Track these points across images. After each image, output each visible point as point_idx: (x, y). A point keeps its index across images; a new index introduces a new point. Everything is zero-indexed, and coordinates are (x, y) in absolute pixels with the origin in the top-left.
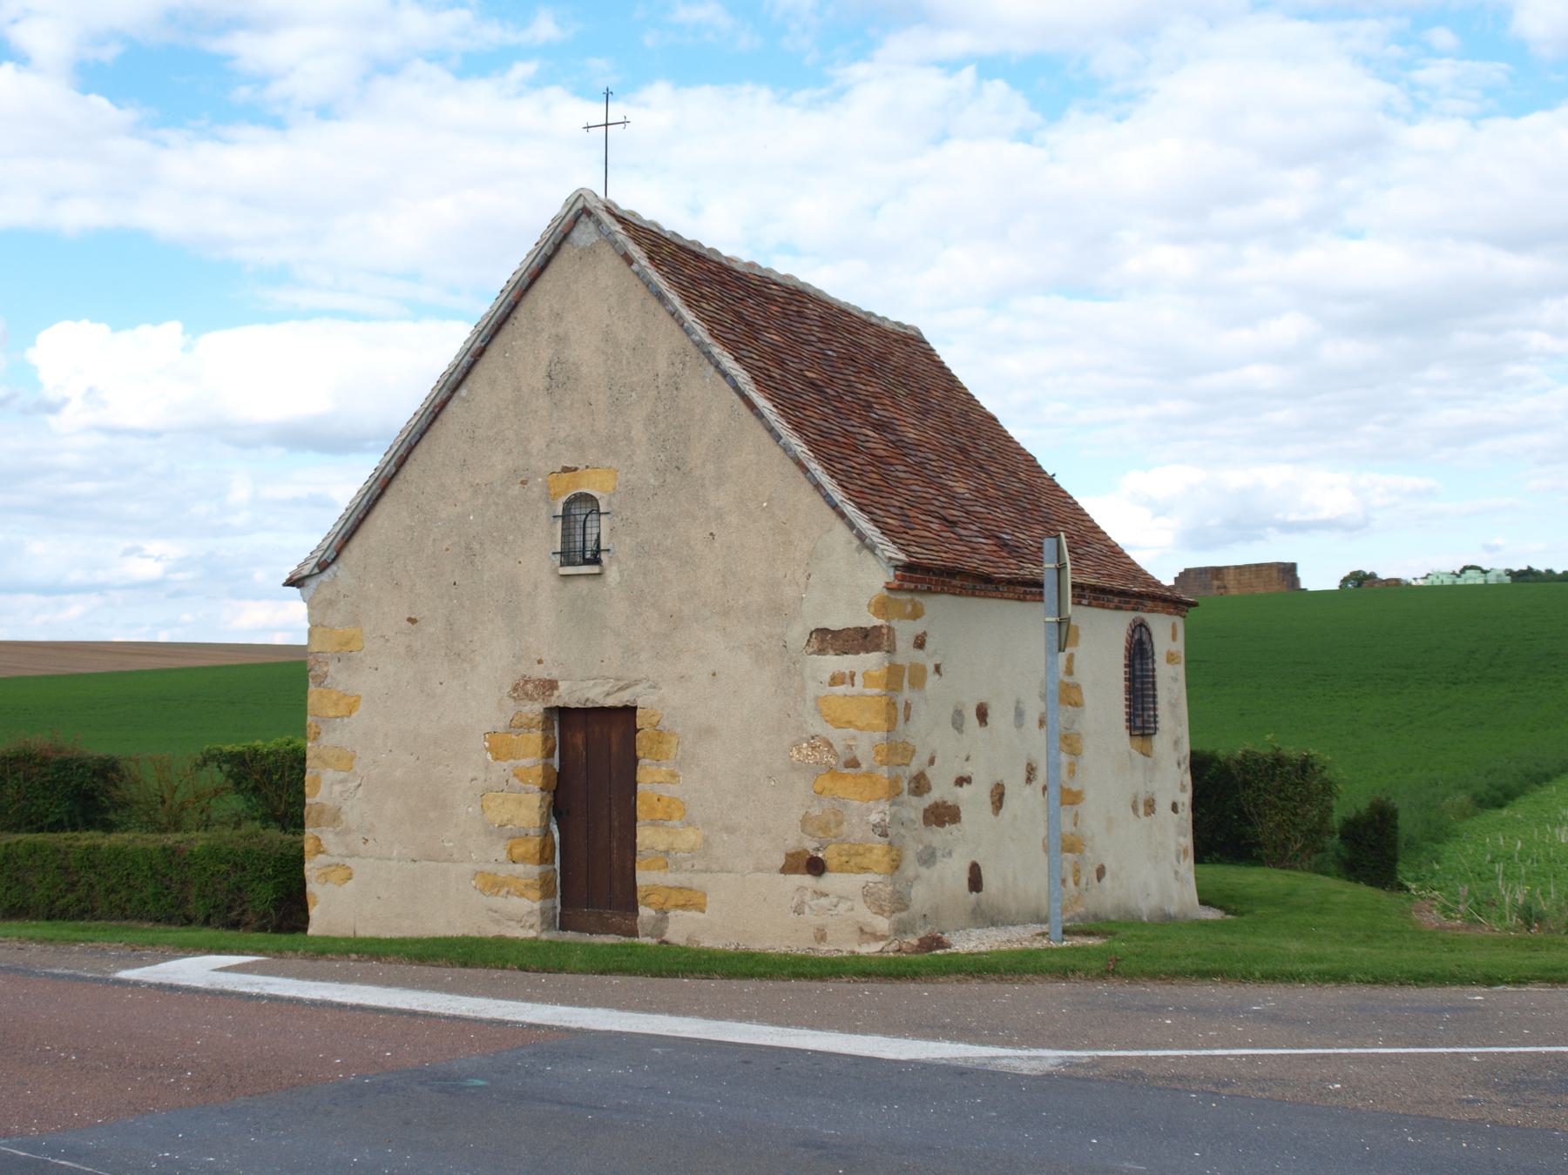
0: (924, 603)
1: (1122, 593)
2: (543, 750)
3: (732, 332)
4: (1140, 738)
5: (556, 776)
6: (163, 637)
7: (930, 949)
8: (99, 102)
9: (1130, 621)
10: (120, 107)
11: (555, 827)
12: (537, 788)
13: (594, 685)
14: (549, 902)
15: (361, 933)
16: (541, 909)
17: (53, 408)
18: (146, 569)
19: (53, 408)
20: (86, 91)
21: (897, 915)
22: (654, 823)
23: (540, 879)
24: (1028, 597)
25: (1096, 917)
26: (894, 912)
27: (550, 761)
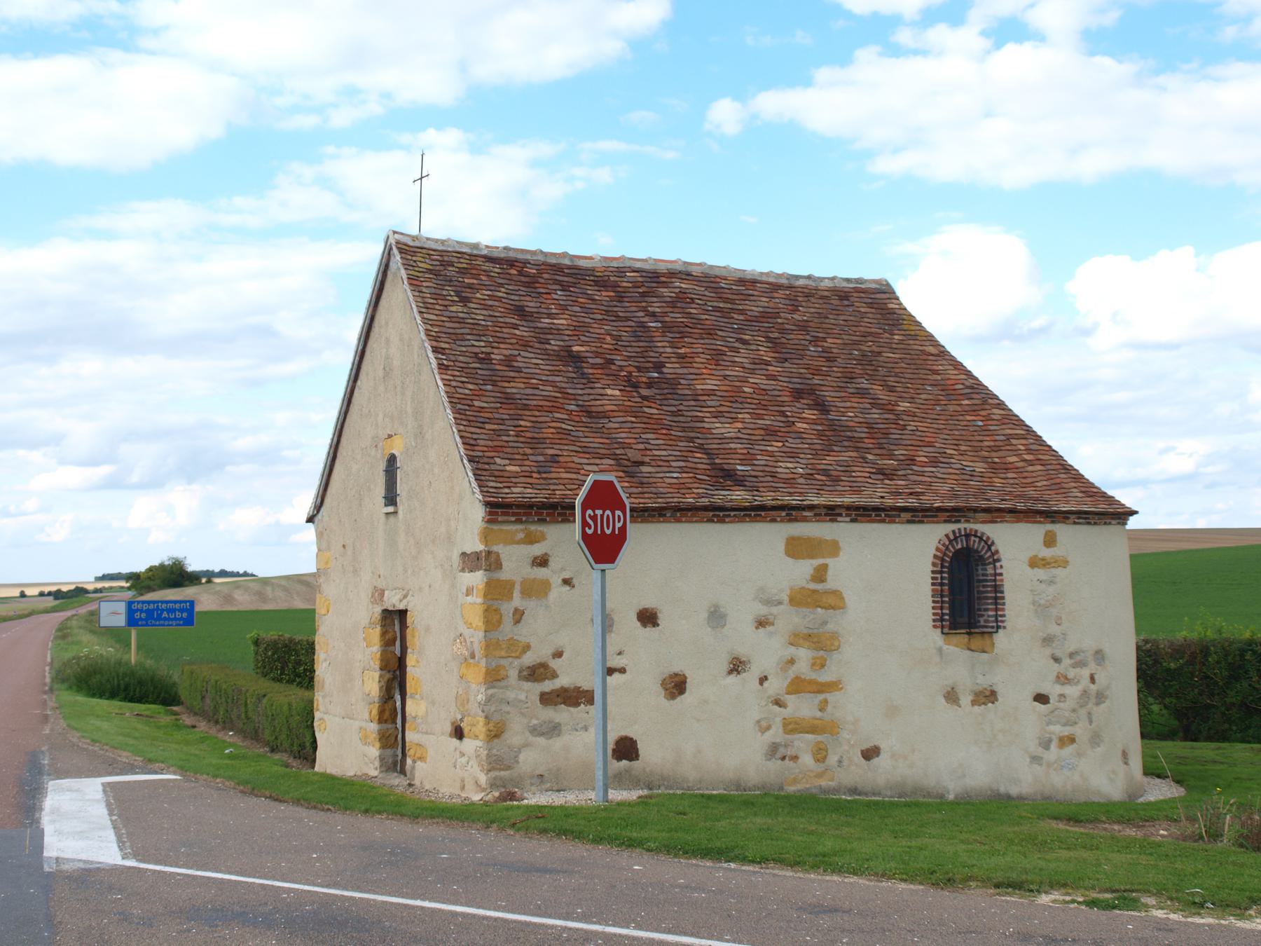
0: (545, 530)
1: (1012, 511)
2: (381, 641)
3: (577, 304)
4: (966, 636)
5: (397, 660)
6: (1201, 524)
7: (505, 800)
8: (1106, 61)
9: (1044, 532)
10: (1120, 62)
11: (399, 697)
12: (377, 667)
13: (396, 593)
14: (389, 752)
15: (328, 771)
16: (380, 756)
17: (1086, 332)
18: (1179, 464)
19: (1086, 332)
20: (1092, 53)
21: (493, 774)
22: (411, 697)
23: (379, 734)
24: (727, 520)
25: (738, 787)
26: (490, 771)
27: (391, 648)
